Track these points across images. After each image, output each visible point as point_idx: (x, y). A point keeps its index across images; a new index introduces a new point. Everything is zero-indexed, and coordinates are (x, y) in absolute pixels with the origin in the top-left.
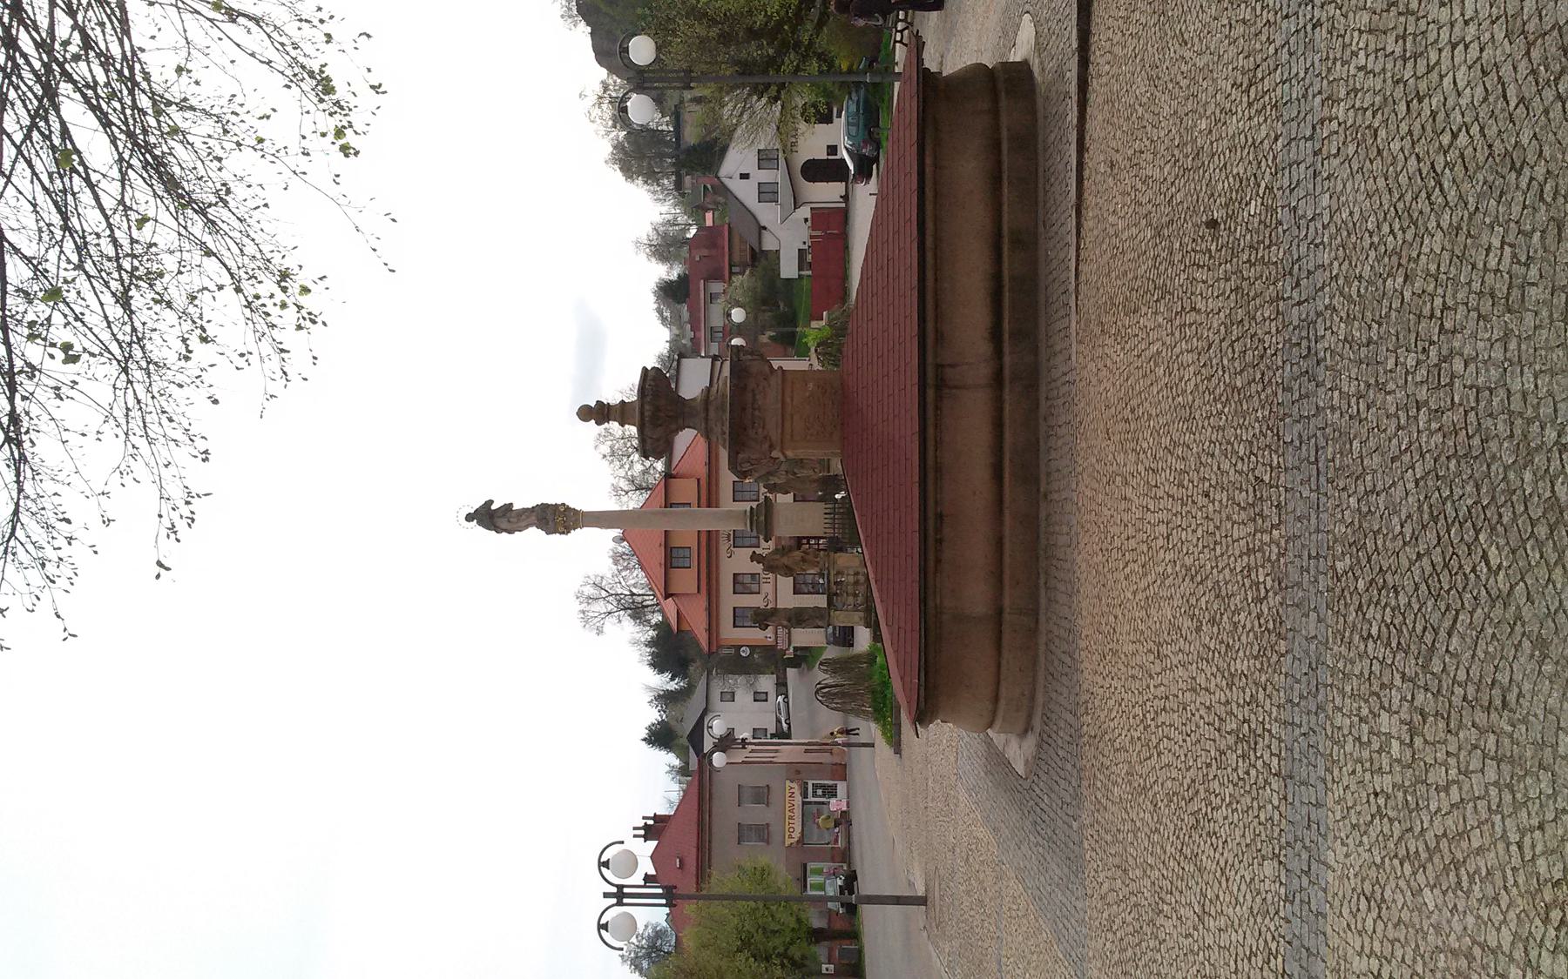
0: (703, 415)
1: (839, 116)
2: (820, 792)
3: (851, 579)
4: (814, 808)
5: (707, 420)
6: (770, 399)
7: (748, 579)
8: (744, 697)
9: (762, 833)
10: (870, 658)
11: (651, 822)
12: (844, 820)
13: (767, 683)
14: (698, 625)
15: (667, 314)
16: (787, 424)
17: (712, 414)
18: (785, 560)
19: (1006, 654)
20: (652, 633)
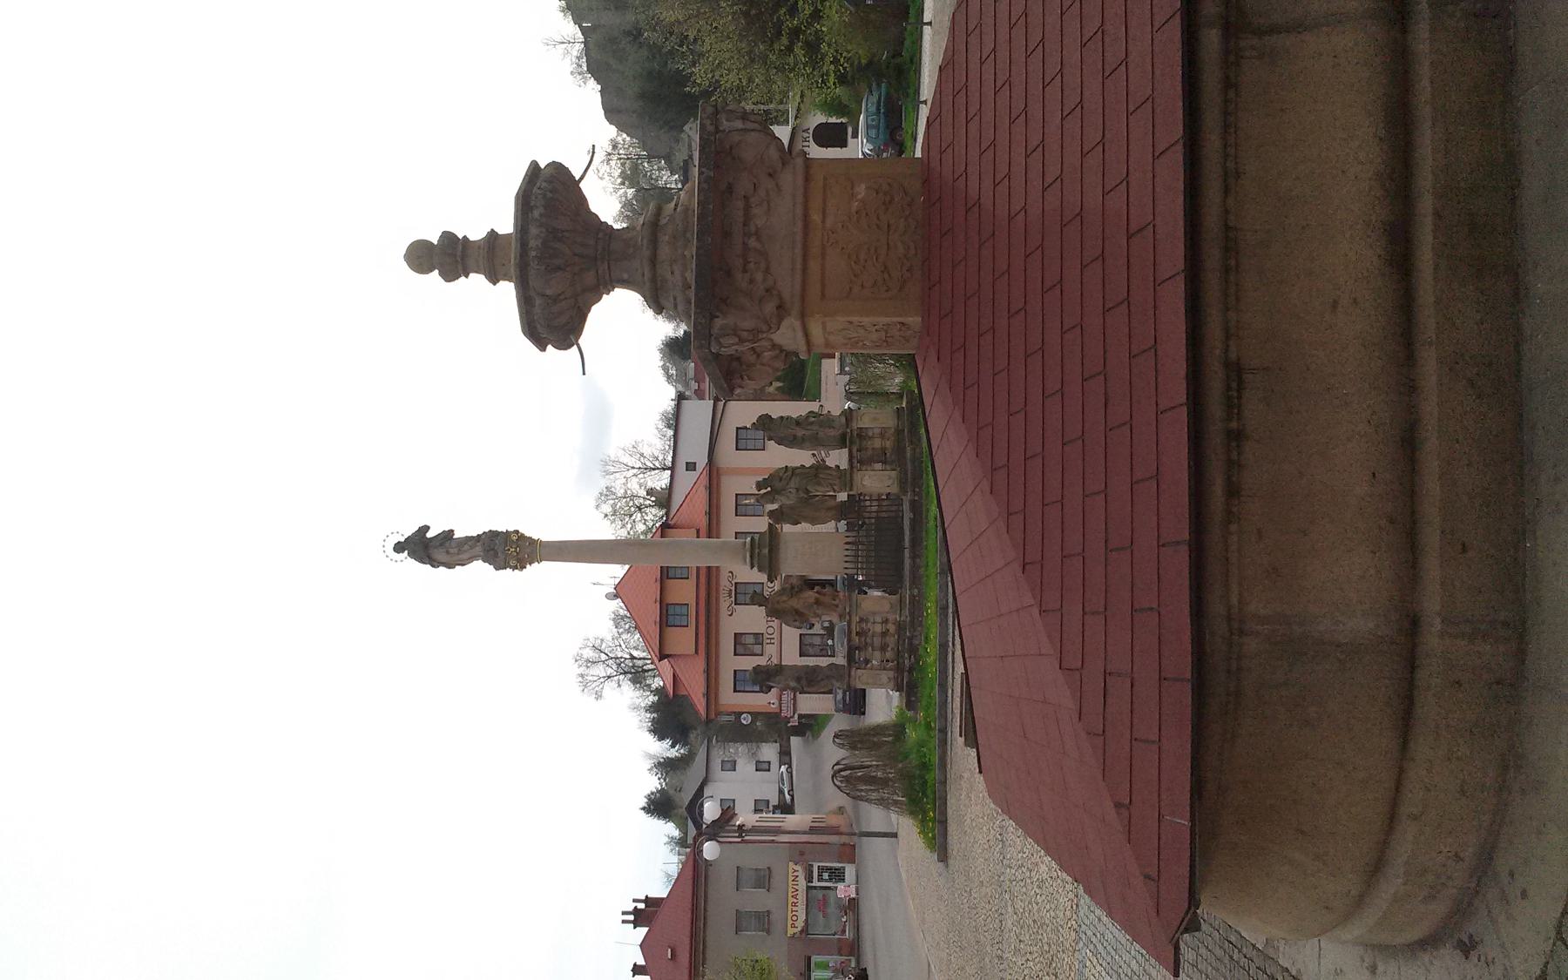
0: (646, 253)
1: (855, 135)
2: (826, 876)
3: (878, 628)
4: (820, 894)
5: (653, 261)
6: (779, 215)
7: (750, 640)
8: (745, 767)
9: (763, 921)
10: (898, 730)
11: (641, 906)
12: (853, 905)
13: (769, 752)
14: (695, 688)
15: (673, 372)
16: (814, 266)
17: (665, 251)
18: (795, 603)
19: (1423, 748)
20: (652, 699)
